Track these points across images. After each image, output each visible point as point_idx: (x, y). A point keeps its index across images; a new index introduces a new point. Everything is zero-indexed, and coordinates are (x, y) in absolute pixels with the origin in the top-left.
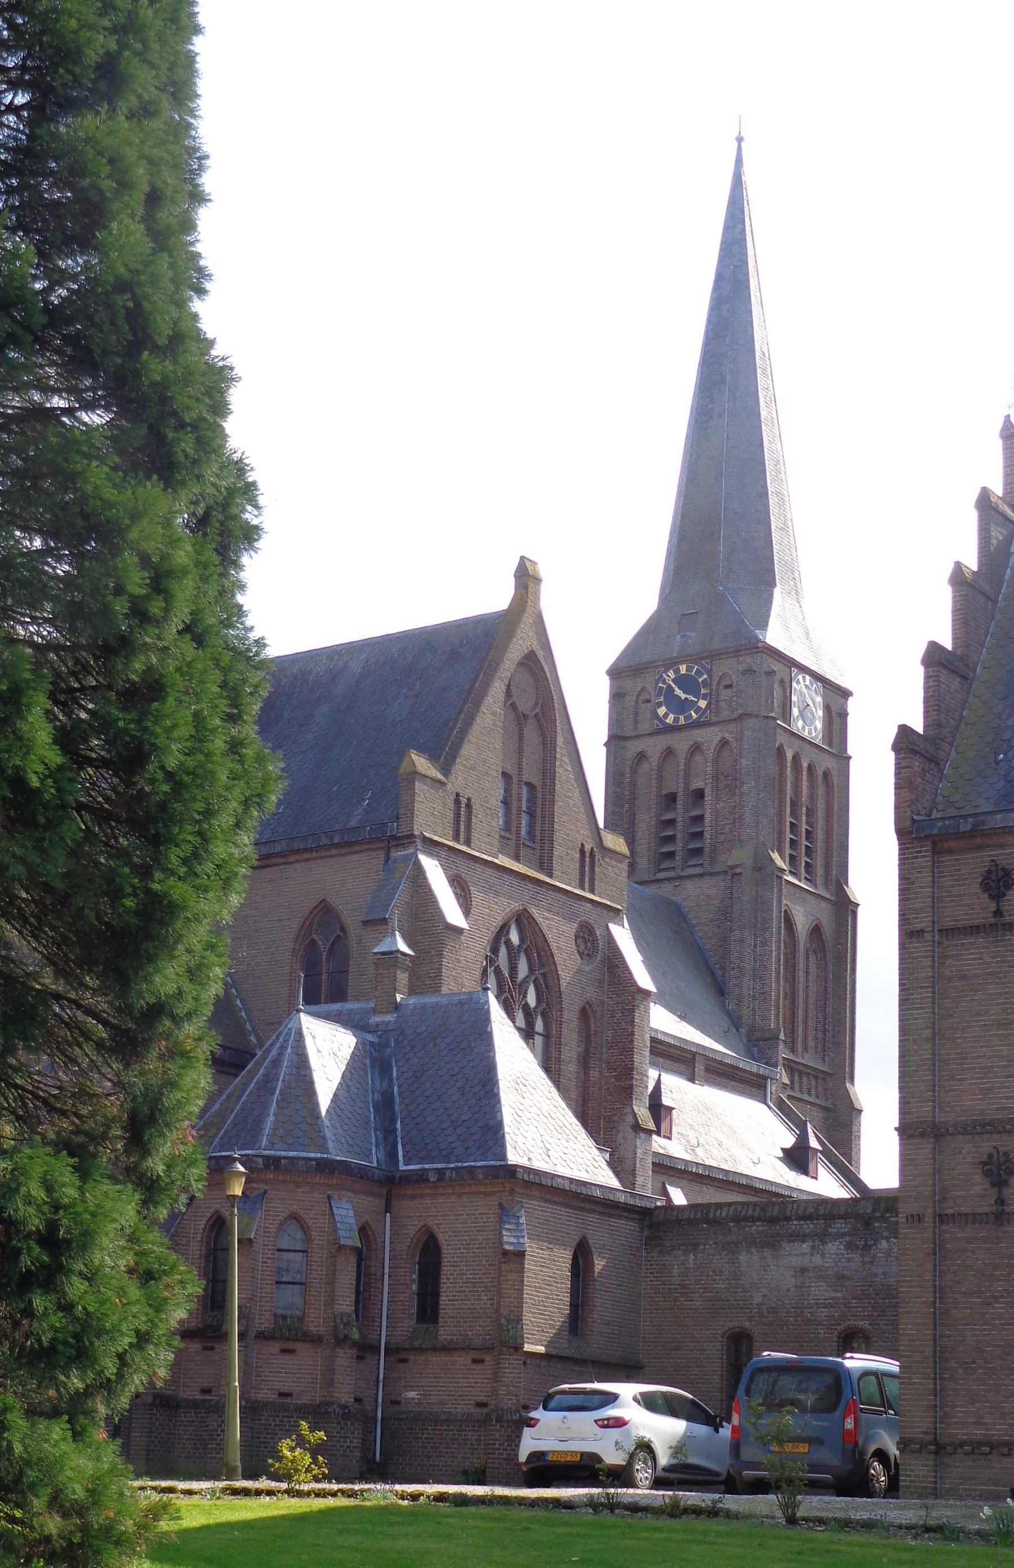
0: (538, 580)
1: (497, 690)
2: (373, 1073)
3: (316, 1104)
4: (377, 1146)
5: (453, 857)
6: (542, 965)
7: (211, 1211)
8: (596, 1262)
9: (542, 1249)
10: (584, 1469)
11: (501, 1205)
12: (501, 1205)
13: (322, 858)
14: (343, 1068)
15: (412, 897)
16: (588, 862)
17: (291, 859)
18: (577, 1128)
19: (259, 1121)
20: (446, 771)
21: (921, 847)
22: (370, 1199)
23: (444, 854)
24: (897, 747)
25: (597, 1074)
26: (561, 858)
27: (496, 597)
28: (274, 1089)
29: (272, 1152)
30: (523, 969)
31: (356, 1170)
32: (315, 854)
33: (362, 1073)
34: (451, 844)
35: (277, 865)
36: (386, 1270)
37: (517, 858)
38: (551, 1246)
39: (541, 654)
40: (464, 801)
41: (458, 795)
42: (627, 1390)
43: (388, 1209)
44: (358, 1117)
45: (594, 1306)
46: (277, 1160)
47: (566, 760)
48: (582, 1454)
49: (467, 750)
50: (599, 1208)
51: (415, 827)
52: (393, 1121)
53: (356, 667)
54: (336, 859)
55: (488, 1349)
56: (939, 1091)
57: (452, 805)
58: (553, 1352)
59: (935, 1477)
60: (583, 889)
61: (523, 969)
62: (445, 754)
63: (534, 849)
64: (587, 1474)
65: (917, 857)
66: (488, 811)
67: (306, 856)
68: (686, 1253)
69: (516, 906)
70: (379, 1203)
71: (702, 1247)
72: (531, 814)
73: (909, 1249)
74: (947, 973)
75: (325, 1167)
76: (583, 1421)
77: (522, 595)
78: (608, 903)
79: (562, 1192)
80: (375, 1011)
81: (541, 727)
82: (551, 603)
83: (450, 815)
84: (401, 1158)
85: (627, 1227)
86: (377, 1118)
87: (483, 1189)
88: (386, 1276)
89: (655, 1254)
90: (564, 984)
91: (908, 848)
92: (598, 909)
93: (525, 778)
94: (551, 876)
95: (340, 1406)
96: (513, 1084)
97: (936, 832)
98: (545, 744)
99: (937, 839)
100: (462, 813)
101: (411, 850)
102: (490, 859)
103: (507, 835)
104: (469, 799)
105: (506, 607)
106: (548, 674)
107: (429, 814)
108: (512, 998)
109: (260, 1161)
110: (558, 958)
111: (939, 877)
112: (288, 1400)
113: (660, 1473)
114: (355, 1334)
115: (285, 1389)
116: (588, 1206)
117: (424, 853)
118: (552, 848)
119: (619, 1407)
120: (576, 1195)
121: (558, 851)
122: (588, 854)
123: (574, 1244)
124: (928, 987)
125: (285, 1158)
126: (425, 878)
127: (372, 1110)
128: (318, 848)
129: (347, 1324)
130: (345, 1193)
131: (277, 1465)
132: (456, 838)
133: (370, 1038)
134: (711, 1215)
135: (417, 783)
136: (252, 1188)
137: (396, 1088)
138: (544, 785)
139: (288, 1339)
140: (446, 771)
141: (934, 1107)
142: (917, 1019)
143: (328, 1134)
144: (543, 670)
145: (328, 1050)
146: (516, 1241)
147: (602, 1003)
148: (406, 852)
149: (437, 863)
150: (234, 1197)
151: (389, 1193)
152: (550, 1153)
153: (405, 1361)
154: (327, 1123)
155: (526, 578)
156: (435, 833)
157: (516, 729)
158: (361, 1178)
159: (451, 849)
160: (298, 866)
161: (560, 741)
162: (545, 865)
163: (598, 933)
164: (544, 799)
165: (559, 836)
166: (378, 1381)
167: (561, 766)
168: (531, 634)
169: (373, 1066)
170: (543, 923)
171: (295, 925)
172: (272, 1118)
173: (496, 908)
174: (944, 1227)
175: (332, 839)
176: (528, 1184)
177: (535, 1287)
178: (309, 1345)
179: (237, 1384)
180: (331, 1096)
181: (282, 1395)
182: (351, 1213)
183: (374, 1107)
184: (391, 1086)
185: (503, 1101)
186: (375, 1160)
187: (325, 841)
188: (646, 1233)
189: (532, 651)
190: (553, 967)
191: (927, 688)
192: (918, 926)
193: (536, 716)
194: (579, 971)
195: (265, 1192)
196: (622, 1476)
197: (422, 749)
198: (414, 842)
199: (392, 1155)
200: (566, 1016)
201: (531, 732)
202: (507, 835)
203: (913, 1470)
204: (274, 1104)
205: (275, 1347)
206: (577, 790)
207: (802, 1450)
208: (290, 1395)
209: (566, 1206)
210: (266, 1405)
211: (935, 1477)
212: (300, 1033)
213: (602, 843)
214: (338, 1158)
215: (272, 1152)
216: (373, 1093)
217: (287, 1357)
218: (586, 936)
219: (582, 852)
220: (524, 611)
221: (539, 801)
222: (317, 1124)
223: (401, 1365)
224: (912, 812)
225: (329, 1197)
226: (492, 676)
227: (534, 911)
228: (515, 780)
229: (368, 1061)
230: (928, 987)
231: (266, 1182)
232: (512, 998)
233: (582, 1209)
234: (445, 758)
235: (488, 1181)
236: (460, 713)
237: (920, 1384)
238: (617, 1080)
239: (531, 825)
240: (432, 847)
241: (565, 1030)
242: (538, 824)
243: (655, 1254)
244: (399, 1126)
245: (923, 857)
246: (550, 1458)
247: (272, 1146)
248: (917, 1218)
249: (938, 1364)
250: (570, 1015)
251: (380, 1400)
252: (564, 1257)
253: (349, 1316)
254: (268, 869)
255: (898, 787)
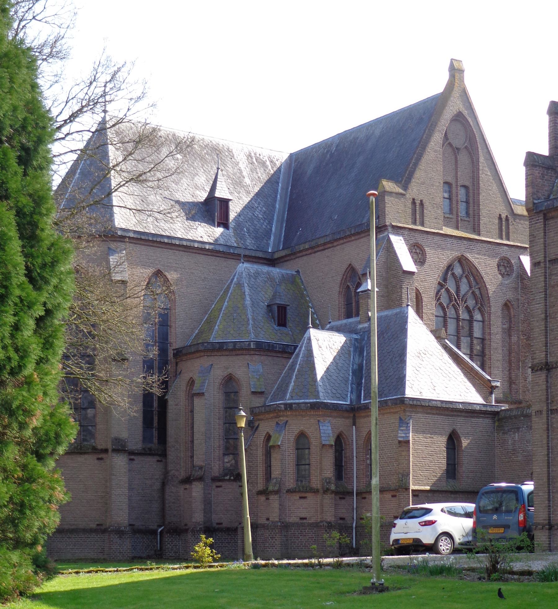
0: (462, 71)
1: (437, 138)
2: (354, 355)
3: (315, 375)
4: (352, 392)
5: (413, 234)
6: (477, 284)
7: (265, 432)
8: (463, 441)
9: (427, 438)
10: (417, 547)
11: (400, 419)
12: (400, 419)
13: (348, 242)
14: (335, 354)
15: (387, 258)
16: (504, 225)
17: (335, 244)
18: (458, 373)
19: (287, 386)
20: (405, 188)
21: (539, 217)
22: (343, 420)
23: (406, 232)
24: (526, 164)
25: (516, 339)
26: (485, 224)
27: (435, 85)
28: (295, 369)
29: (292, 401)
30: (464, 288)
31: (331, 407)
32: (345, 240)
33: (347, 356)
34: (410, 227)
35: (330, 248)
36: (355, 455)
37: (457, 228)
38: (433, 436)
39: (465, 113)
40: (418, 202)
41: (414, 199)
42: (437, 507)
43: (354, 424)
44: (341, 379)
45: (463, 464)
46: (291, 405)
47: (487, 169)
48: (413, 539)
49: (419, 174)
50: (463, 414)
51: (387, 221)
52: (361, 379)
53: (377, 132)
54: (354, 242)
55: (396, 490)
56: (550, 346)
57: (410, 206)
58: (434, 488)
59: (549, 541)
60: (502, 239)
61: (464, 288)
62: (404, 178)
63: (469, 221)
64: (424, 548)
65: (537, 223)
66: (435, 205)
67: (342, 242)
68: (514, 433)
69: (457, 254)
70: (349, 421)
71: (521, 429)
72: (467, 202)
73: (536, 429)
74: (552, 283)
75: (315, 406)
76: (413, 523)
77: (451, 81)
78: (519, 244)
79: (437, 408)
80: (360, 322)
81: (470, 153)
82: (472, 83)
83: (409, 211)
84: (362, 398)
85: (485, 422)
86: (354, 377)
87: (392, 411)
88: (355, 458)
89: (501, 434)
90: (490, 293)
91: (533, 219)
92: (513, 249)
93: (460, 183)
94: (479, 235)
95: (326, 522)
96: (417, 354)
97: (544, 208)
98: (473, 162)
99: (545, 212)
100: (418, 209)
101: (386, 233)
102: (436, 231)
103: (451, 216)
104: (421, 201)
105: (442, 91)
106: (471, 123)
107: (396, 212)
108: (458, 304)
109: (282, 406)
110: (486, 279)
111: (548, 232)
112: (305, 521)
113: (457, 545)
114: (333, 487)
115: (303, 516)
116: (455, 413)
117: (393, 234)
118: (479, 219)
119: (431, 515)
120: (447, 409)
121: (484, 220)
122: (504, 220)
123: (448, 434)
124: (542, 292)
125: (295, 404)
126: (393, 248)
127: (351, 374)
128: (346, 237)
129: (329, 482)
130: (328, 418)
131: (195, 555)
132: (414, 223)
133: (355, 336)
134: (525, 412)
135: (386, 197)
136: (281, 420)
137: (365, 361)
138: (473, 185)
139: (302, 492)
140: (405, 188)
141: (547, 354)
142: (538, 309)
143: (320, 389)
144: (468, 121)
145: (325, 346)
146: (405, 436)
147: (518, 300)
148: (384, 235)
149: (401, 238)
150: (242, 427)
151: (354, 416)
152: (435, 388)
153: (365, 498)
154: (321, 384)
155: (456, 72)
156: (400, 222)
157: (453, 157)
158: (335, 410)
159: (410, 229)
160: (338, 247)
161: (482, 159)
162: (476, 230)
163: (513, 262)
164: (474, 194)
165: (484, 212)
166: (353, 509)
167: (483, 173)
168: (458, 102)
169: (355, 351)
170: (475, 262)
171: (339, 278)
172: (292, 384)
173: (439, 258)
174: (553, 416)
175: (351, 232)
176: (412, 406)
177: (422, 457)
178: (313, 494)
179: (248, 516)
180: (325, 369)
181: (302, 519)
182: (330, 428)
183: (353, 373)
184: (363, 361)
185: (408, 364)
186: (349, 400)
187: (348, 233)
188: (496, 424)
189: (460, 112)
190: (483, 284)
191: (550, 127)
192: (538, 260)
193: (466, 147)
194: (501, 284)
195: (287, 421)
196: (432, 548)
197: (390, 178)
198: (387, 229)
199: (359, 397)
200: (493, 309)
201: (463, 158)
202: (451, 216)
203: (539, 539)
204: (294, 377)
205: (296, 496)
206: (495, 185)
207: (501, 531)
208: (305, 519)
209: (442, 415)
210: (293, 524)
211: (549, 541)
212: (309, 339)
213: (513, 212)
214: (325, 401)
215: (292, 401)
216: (353, 365)
217: (303, 501)
218: (506, 265)
219: (500, 218)
220: (452, 90)
221: (471, 195)
222: (315, 385)
223: (364, 500)
224: (533, 199)
225: (319, 421)
226: (433, 130)
227: (469, 256)
228: (454, 186)
229: (352, 349)
230: (542, 292)
231: (287, 416)
232: (458, 304)
233: (452, 416)
234: (405, 180)
235: (393, 406)
236: (414, 153)
237: (542, 496)
238: (527, 341)
239: (468, 208)
240: (398, 230)
241: (493, 318)
242: (471, 209)
243: (501, 434)
244: (363, 381)
245: (540, 222)
246: (400, 542)
247: (292, 398)
248: (539, 412)
249: (548, 484)
250: (496, 308)
251: (355, 518)
252: (441, 442)
253: (330, 478)
254: (326, 250)
255: (527, 186)
